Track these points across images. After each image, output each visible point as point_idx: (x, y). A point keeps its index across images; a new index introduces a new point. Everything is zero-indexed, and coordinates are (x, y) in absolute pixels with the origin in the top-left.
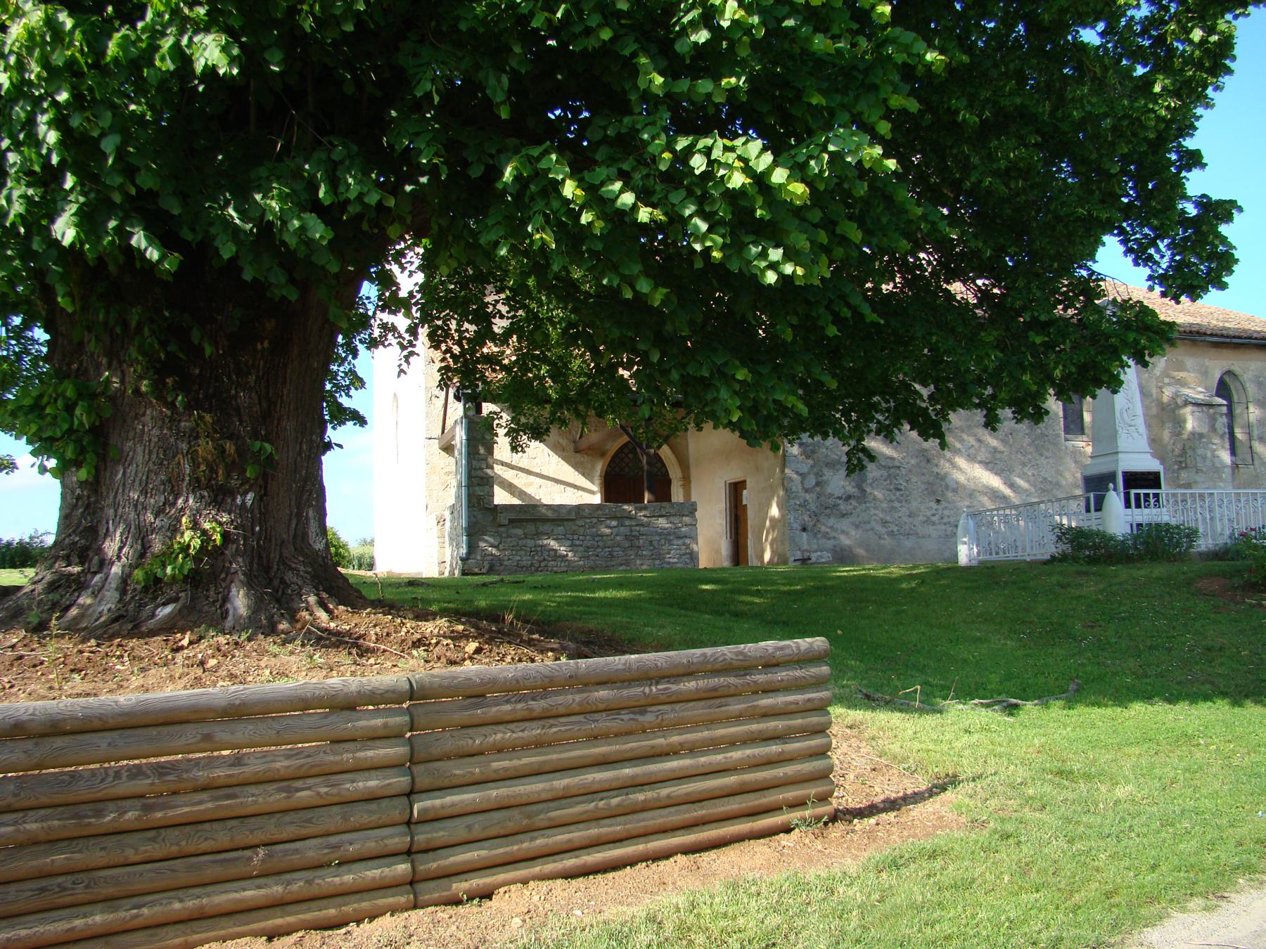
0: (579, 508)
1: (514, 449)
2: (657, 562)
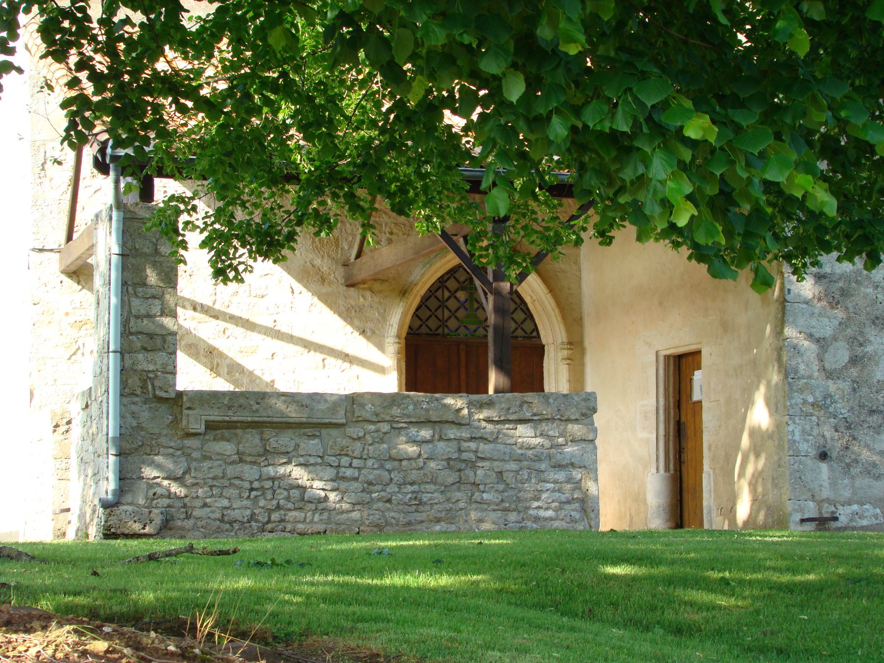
0: (353, 400)
1: (220, 274)
2: (513, 517)
